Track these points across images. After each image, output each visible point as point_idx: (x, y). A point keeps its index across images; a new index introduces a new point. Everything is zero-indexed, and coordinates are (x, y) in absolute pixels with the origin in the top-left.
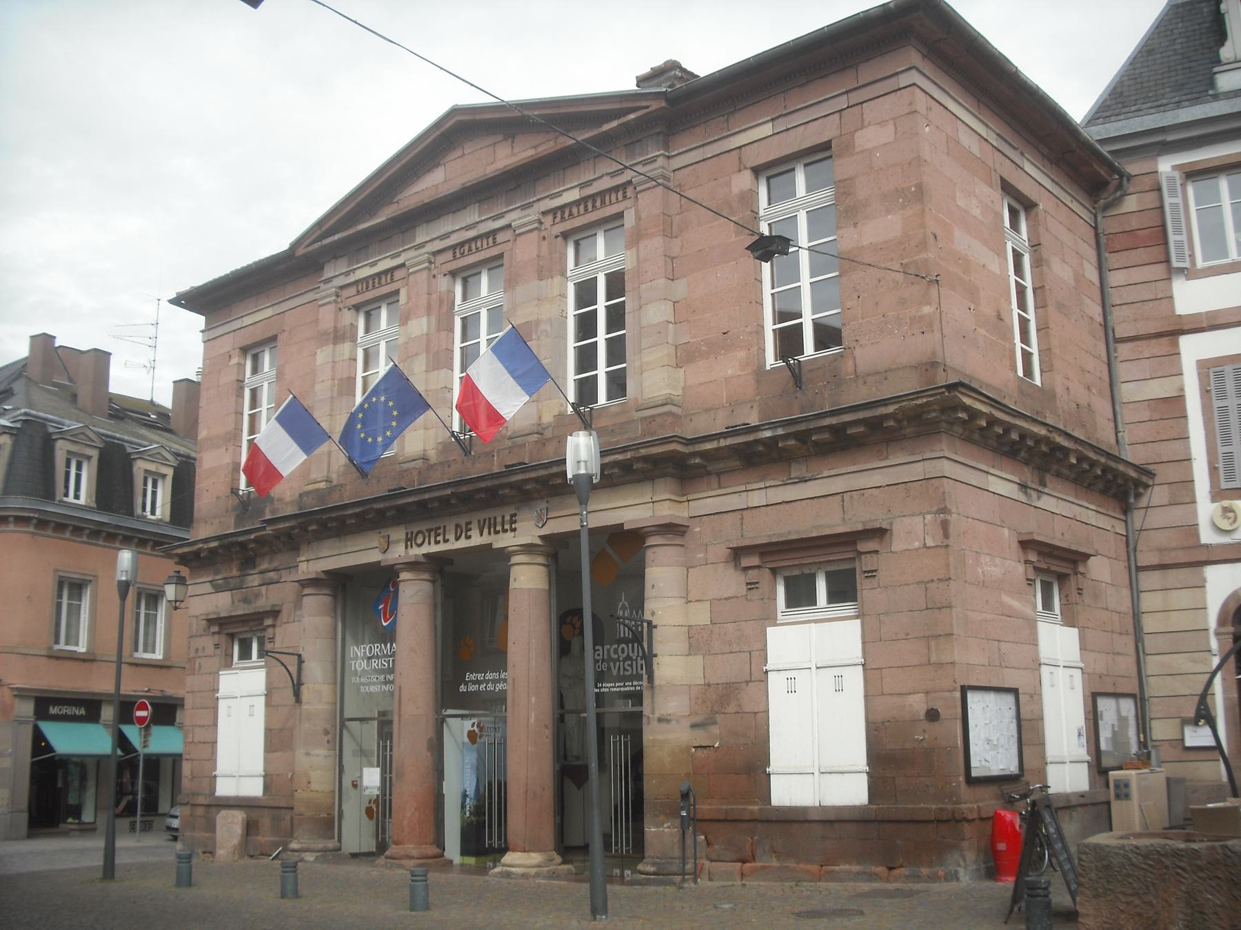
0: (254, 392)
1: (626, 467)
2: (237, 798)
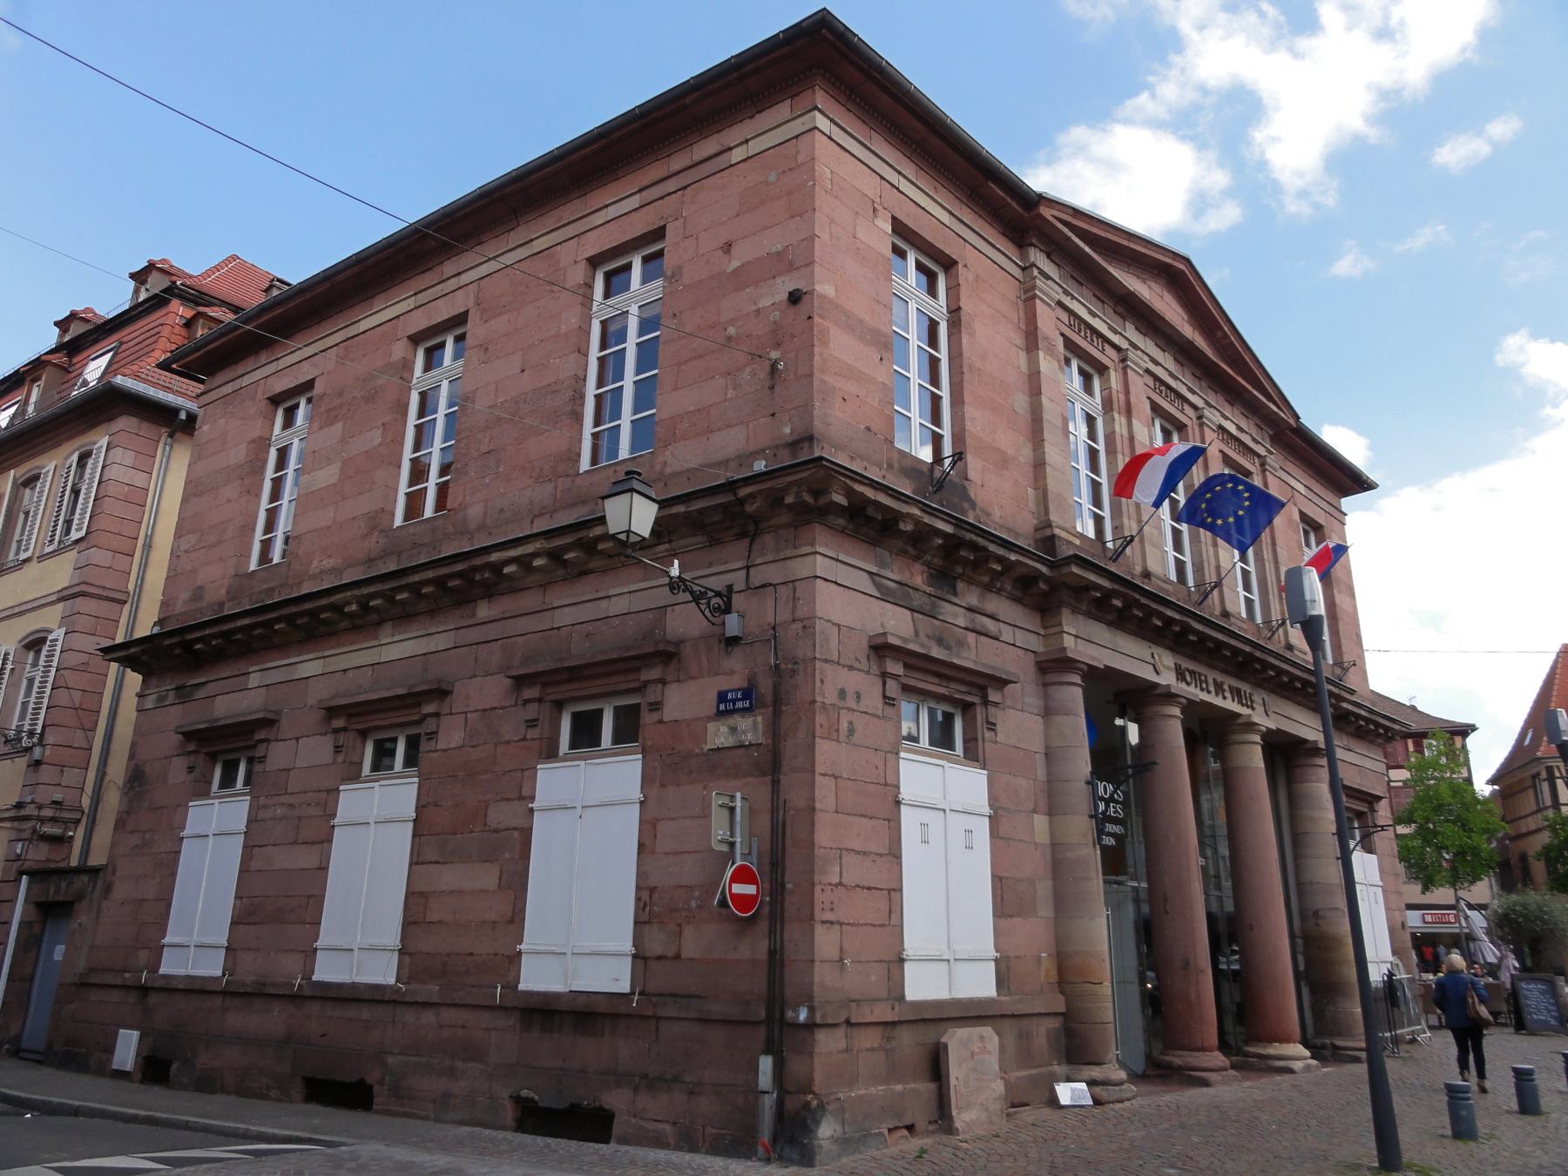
0: (283, 454)
1: (696, 523)
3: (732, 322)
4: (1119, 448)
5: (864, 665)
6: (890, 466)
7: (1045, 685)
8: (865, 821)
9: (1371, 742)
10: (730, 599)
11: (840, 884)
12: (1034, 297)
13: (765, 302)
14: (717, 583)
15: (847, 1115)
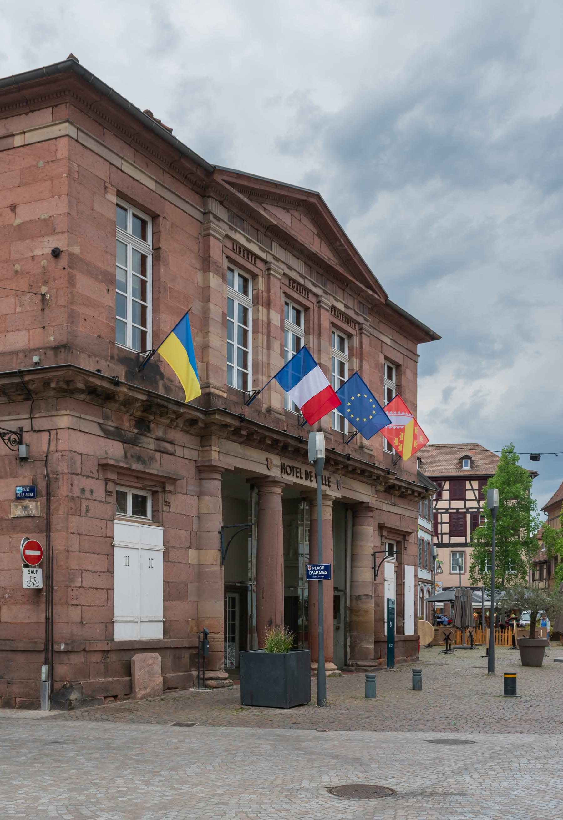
2: (141, 642)
3: (18, 261)
4: (260, 330)
5: (95, 475)
6: (112, 358)
7: (200, 479)
8: (96, 556)
9: (411, 500)
10: (21, 435)
11: (81, 587)
12: (209, 235)
13: (38, 252)
14: (13, 426)
15: (84, 691)
